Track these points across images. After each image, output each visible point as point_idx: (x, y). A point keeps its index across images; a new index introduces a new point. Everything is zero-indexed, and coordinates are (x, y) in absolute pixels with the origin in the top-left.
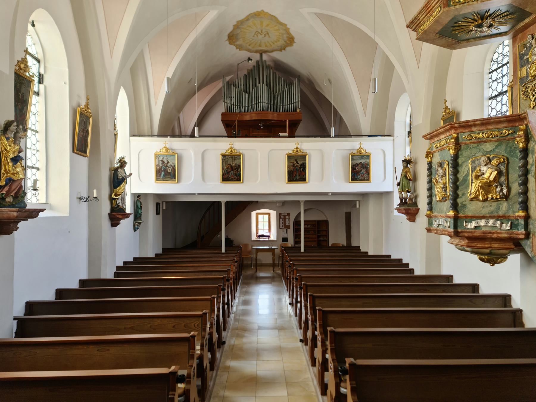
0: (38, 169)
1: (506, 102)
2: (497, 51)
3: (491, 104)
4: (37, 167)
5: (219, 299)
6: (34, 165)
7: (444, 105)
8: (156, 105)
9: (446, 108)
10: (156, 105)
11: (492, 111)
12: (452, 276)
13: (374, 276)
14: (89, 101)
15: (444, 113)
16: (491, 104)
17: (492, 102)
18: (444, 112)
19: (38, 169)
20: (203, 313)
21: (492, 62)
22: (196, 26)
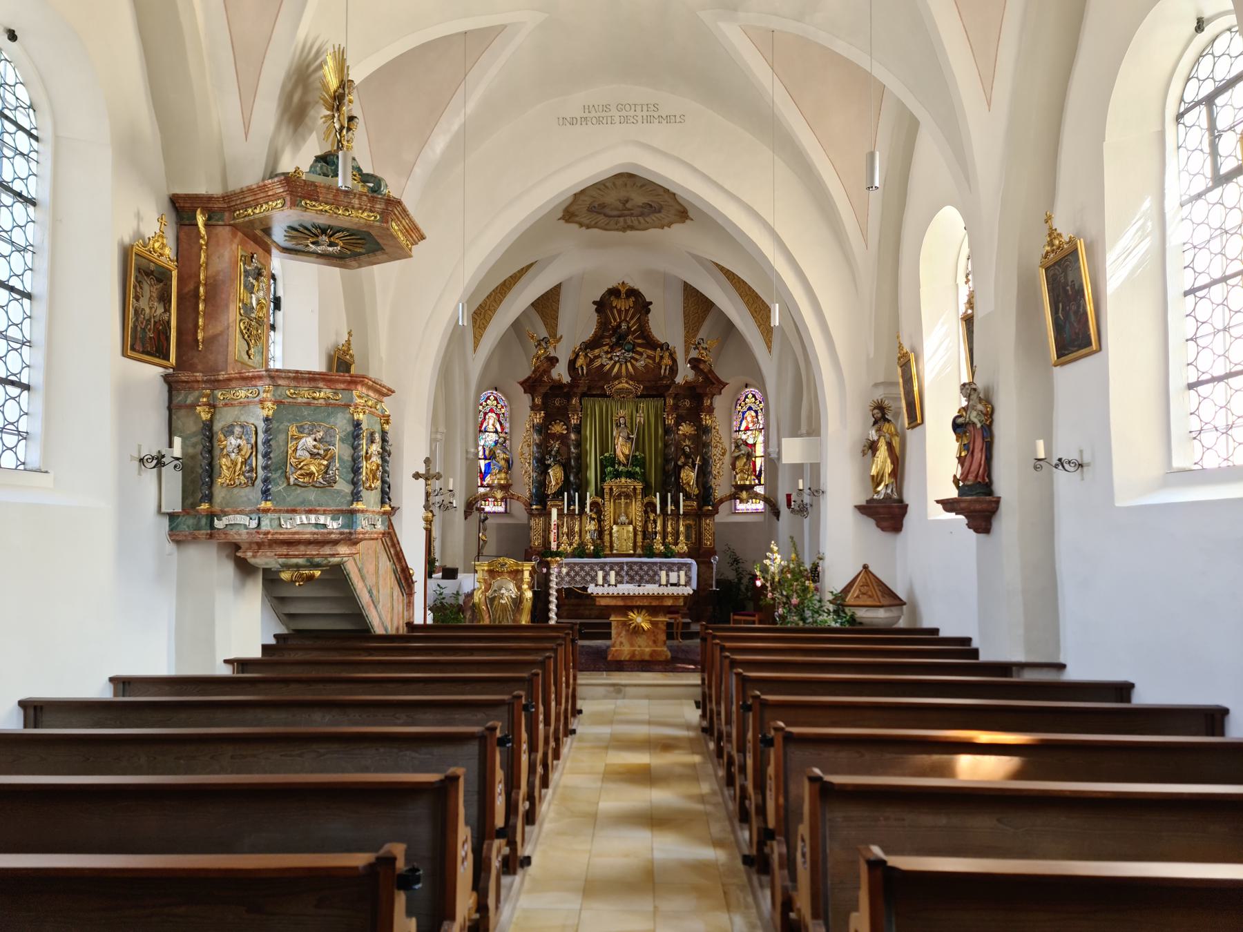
0: (26, 387)
1: (1227, 266)
2: (1196, 76)
3: (1205, 161)
4: (22, 381)
5: (511, 817)
6: (15, 375)
7: (1047, 226)
8: (475, 351)
9: (1053, 234)
10: (475, 351)
11: (1193, 261)
12: (1224, 712)
13: (398, 701)
14: (351, 338)
15: (1048, 248)
16: (1205, 161)
17: (1192, 206)
18: (1049, 245)
19: (26, 387)
20: (378, 859)
21: (1183, 103)
22: (466, 75)
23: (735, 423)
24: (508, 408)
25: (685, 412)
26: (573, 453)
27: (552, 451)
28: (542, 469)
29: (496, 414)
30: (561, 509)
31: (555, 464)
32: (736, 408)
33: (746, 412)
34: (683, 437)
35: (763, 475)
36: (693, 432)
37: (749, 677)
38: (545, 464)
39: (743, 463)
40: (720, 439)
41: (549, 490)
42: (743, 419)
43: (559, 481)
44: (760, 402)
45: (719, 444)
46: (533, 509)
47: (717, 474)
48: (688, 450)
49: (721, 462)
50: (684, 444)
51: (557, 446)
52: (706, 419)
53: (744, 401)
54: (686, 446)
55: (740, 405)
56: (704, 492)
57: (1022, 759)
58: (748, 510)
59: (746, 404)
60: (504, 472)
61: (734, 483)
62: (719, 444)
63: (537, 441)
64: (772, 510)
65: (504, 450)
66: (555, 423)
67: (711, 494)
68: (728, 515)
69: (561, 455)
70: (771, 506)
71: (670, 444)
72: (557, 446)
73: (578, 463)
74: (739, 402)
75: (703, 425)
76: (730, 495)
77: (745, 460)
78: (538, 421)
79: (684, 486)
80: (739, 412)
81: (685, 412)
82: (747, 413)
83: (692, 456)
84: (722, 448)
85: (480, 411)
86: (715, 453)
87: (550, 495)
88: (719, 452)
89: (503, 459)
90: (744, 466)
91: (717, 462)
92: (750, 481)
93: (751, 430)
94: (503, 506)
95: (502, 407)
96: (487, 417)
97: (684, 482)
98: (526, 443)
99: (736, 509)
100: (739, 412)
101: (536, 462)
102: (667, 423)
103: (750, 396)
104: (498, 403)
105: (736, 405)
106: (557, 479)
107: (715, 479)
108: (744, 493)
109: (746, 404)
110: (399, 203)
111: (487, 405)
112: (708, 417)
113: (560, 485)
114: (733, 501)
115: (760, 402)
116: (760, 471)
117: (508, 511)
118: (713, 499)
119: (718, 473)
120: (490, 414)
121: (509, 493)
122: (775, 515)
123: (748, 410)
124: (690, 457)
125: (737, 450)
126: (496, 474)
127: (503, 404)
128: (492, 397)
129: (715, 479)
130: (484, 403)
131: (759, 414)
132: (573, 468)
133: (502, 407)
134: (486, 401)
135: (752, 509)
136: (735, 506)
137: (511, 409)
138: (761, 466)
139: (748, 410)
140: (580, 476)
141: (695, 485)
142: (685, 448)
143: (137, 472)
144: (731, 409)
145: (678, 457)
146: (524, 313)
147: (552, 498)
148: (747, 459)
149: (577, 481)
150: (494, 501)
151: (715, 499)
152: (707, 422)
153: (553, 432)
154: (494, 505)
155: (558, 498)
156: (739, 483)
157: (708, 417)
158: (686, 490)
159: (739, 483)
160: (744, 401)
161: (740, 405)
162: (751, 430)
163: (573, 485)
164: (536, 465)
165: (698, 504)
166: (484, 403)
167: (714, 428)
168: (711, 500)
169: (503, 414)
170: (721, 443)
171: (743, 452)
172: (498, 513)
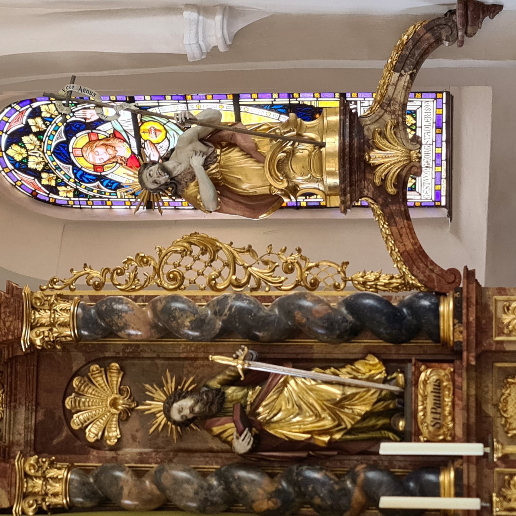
23: (119, 210)
25: (22, 414)
32: (66, 206)
33: (76, 169)
34: (134, 423)
35: (307, 100)
36: (116, 379)
39: (249, 164)
40: (143, 261)
42: (100, 178)
44: (36, 113)
45: (167, 269)
47: (295, 276)
48: (187, 403)
49: (245, 259)
50: (161, 418)
52: (52, 325)
53: (36, 174)
54: (167, 411)
55: (53, 190)
56: (378, 336)
58: (438, 155)
59: (47, 169)
61: (336, 201)
62: (167, 269)
64: (452, 38)
67: (386, 302)
68: (456, 232)
70: (438, 41)
71: (157, 483)
74: (43, 193)
75: (79, 338)
76: (390, 219)
77: (235, 155)
79: (348, 423)
80: (78, 194)
81: (22, 414)
82: (80, 162)
83: (214, 384)
84: (184, 253)
86: (202, 282)
88: (199, 266)
90: (259, 159)
91: (241, 275)
92: (324, 131)
93: (140, 146)
97: (328, 423)
99: (435, 206)
100: (78, 194)
102: (61, 500)
103: (15, 152)
105: (55, 204)
107: (315, 285)
108: (349, 426)
109: (47, 169)
110: (421, 144)
112: (44, 316)
114: (413, 214)
115: (36, 113)
116: (287, 109)
118: (407, 295)
119: (289, 270)
122: (477, 22)
123: (67, 160)
124: (220, 394)
125: (191, 189)
129: (315, 285)
131: (79, 116)
135: (437, 143)
136: (423, 206)
138: (271, 107)
139: (67, 160)
141: (344, 376)
142: (176, 416)
144: (66, 224)
145: (216, 445)
148: (232, 145)
151: (406, 286)
152: (64, 317)
156: (334, 181)
157: (44, 316)
158: (366, 416)
159: (334, 181)
160: (36, 174)
161: (53, 190)
162: (140, 146)
165: (428, 362)
167: (98, 287)
168: (410, 305)
170: (163, 256)
171: (197, 162)
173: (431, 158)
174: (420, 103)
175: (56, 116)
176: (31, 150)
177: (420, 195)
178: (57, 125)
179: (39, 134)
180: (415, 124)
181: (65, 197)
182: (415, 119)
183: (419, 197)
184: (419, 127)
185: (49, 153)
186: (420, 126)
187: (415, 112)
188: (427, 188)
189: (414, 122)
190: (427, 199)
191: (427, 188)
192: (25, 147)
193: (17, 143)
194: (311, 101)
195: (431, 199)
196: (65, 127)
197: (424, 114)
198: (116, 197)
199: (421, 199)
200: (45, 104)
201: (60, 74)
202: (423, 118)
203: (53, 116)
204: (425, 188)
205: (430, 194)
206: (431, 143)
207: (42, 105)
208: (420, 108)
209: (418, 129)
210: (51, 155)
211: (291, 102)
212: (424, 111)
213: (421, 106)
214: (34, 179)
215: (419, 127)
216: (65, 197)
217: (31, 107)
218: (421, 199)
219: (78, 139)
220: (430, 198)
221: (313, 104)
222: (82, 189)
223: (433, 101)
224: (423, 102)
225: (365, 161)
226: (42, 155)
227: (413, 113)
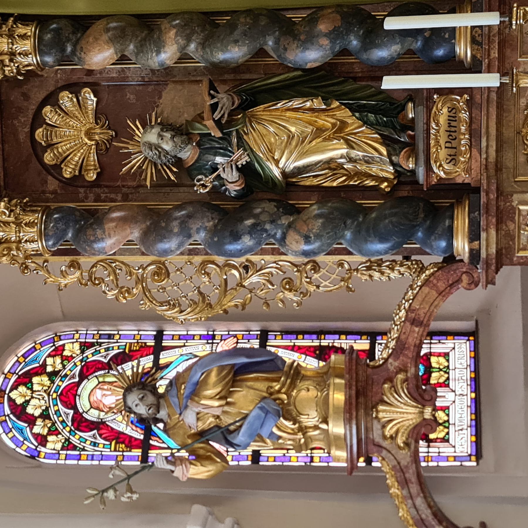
24: (64, 328)
26: (184, 57)
27: (179, 162)
28: (270, 207)
29: (84, 376)
30: (470, 104)
31: (242, 144)
37: (252, 377)
38: (241, 196)
41: (374, 170)
43: (325, 121)
46: (475, 255)
51: (152, 137)
57: (343, 402)
60: (293, 386)
63: (135, 234)
65: (184, 390)
66: (50, 146)
69: (200, 118)
72: (152, 137)
73: (232, 27)
78: (32, 232)
85: (68, 445)
87: (399, 173)
89: (223, 396)
94: (447, 345)
95: (58, 351)
96: (93, 415)
98: (154, 286)
100: (68, 445)
101: (236, 237)
104: (41, 370)
106: (319, 131)
111: (45, 416)
113: (345, 114)
117: (467, 325)
120: (83, 403)
121: (393, 364)
126: (303, 430)
127: (48, 349)
128: (14, 395)
130: (39, 428)
132: (261, 53)
133: (58, 351)
134: (31, 421)
137: (66, 317)
140: (297, 16)
143: (479, 322)
146: (484, 73)
147: (413, 151)
149: (323, 27)
150: (429, 441)
153: (93, 158)
154: (445, 385)
155: (411, 125)
163: (345, 52)
164: (247, 241)
166: (39, 428)
169: (85, 346)
172: (476, 370)
173: (466, 404)
174: (453, 346)
175: (77, 355)
176: (38, 391)
177: (454, 447)
178: (75, 364)
179: (53, 375)
180: (448, 421)
181: (51, 449)
182: (448, 361)
183: (452, 450)
184: (452, 370)
185: (55, 396)
186: (453, 423)
187: (448, 408)
188: (462, 439)
189: (446, 418)
190: (462, 452)
191: (462, 439)
192: (31, 389)
193: (25, 384)
194: (341, 343)
195: (467, 452)
196: (82, 367)
197: (457, 356)
198: (109, 450)
199: (455, 452)
200: (70, 343)
201: (91, 81)
202: (456, 360)
203: (74, 355)
204: (460, 438)
205: (465, 446)
206: (465, 367)
207: (68, 343)
208: (454, 404)
209: (451, 426)
210: (56, 398)
211: (322, 344)
212: (457, 353)
213: (454, 348)
214: (27, 427)
215: (452, 370)
216: (51, 449)
217: (54, 345)
218: (455, 452)
219: (90, 381)
220: (466, 451)
221: (343, 346)
222: (75, 440)
223: (466, 343)
224: (456, 344)
225: (394, 188)
226: (46, 398)
227: (444, 409)
